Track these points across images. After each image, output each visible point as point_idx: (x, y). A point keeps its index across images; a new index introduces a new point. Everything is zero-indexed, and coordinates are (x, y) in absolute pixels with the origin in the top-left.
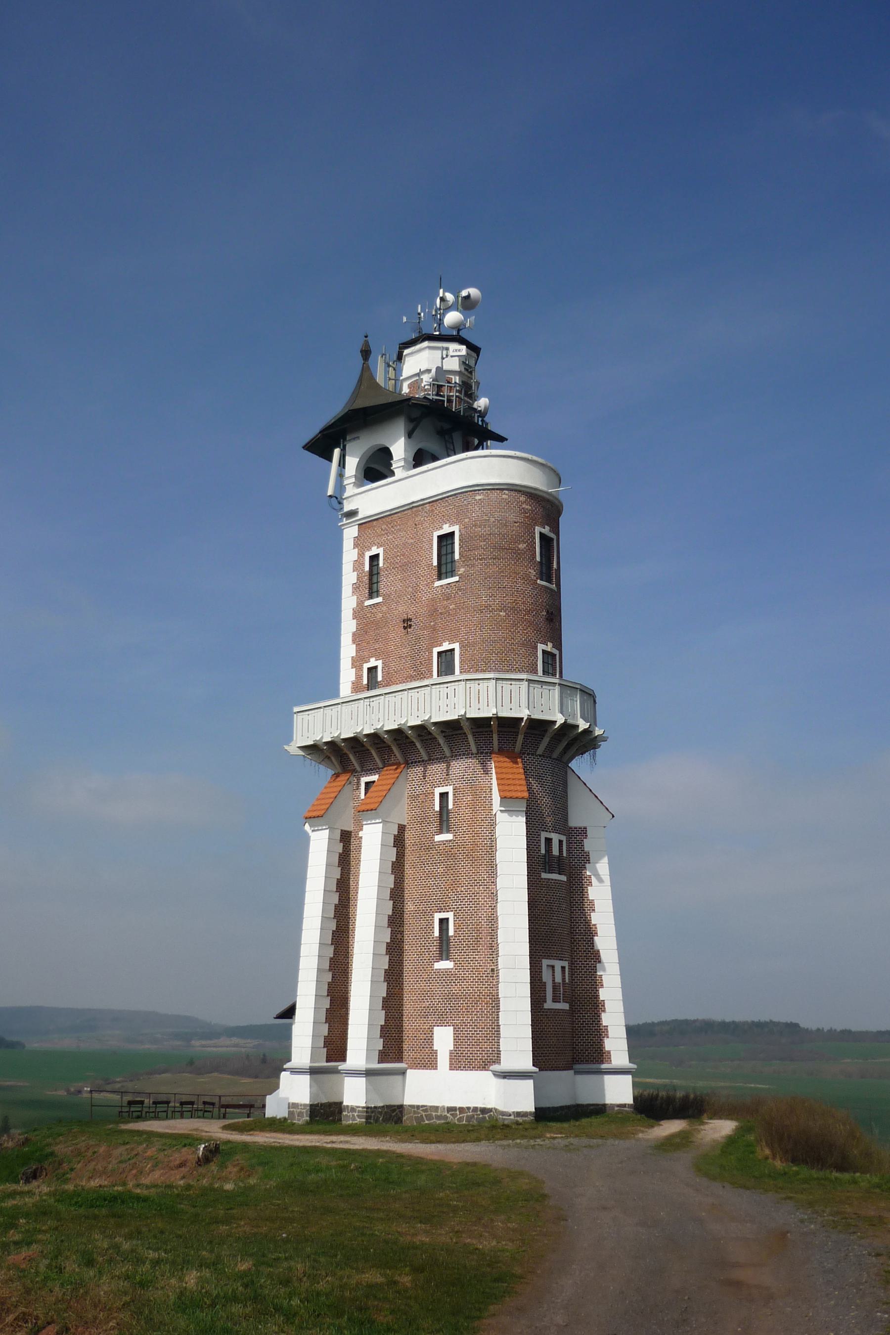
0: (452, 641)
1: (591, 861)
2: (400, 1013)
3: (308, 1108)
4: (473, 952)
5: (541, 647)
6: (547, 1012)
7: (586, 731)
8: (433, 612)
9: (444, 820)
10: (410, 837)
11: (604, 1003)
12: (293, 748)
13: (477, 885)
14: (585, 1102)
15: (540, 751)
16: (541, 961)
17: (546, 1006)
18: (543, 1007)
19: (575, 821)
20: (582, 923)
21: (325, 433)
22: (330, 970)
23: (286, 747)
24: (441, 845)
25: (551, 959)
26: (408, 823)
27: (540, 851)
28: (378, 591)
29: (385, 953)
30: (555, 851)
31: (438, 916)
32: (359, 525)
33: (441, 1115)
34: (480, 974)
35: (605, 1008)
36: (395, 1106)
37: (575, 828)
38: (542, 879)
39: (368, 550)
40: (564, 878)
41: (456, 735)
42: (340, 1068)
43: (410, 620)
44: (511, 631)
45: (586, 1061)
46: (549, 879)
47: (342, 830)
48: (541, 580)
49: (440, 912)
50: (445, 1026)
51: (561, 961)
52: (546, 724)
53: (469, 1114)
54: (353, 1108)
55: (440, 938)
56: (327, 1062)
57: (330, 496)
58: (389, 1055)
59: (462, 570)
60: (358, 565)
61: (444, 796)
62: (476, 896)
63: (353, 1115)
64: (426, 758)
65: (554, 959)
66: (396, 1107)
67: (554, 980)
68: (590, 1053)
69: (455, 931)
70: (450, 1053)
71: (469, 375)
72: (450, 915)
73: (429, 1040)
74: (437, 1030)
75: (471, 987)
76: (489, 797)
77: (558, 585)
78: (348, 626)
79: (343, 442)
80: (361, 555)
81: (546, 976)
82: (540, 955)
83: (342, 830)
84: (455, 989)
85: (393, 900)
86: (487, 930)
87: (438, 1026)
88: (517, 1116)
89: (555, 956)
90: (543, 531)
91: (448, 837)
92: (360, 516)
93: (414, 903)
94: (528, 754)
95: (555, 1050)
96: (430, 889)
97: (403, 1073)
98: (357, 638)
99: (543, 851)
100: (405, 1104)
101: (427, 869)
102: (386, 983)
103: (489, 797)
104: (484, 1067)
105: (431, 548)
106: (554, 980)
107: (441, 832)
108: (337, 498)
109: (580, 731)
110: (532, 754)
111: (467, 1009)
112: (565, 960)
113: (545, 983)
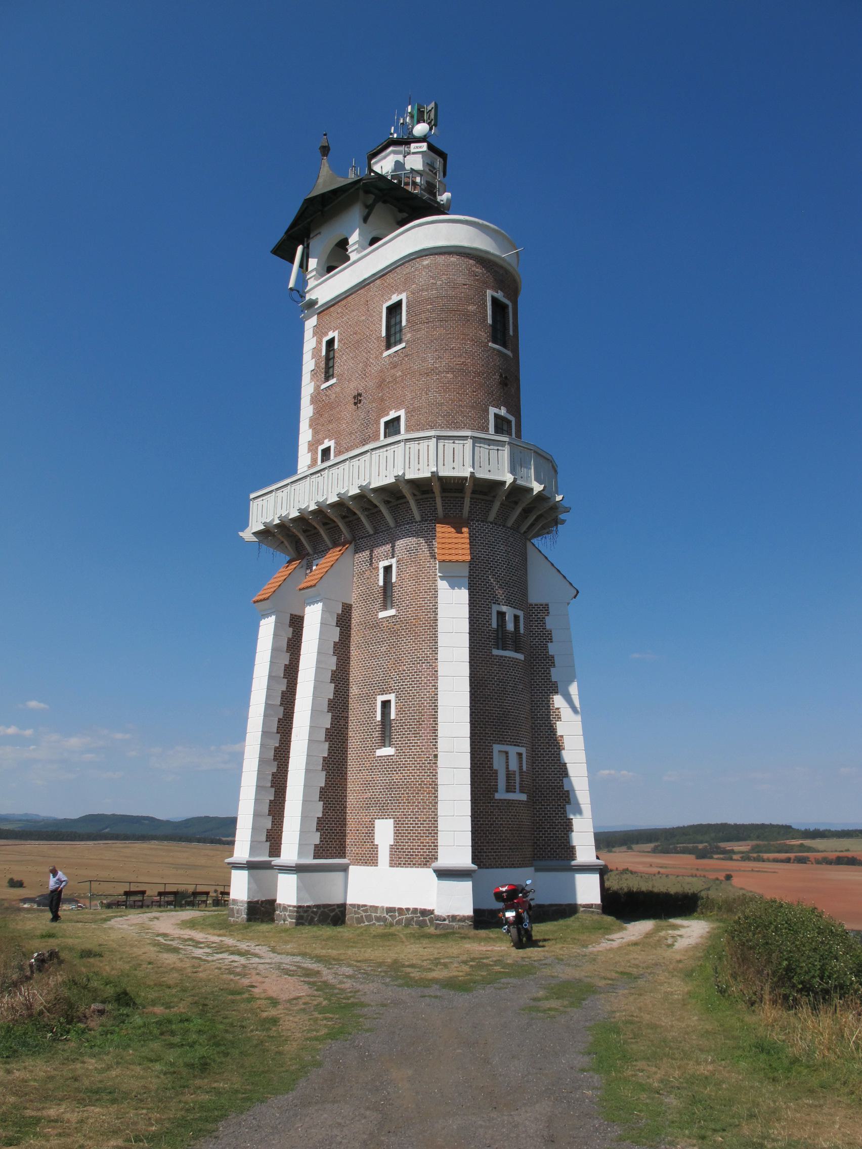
0: (398, 409)
1: (554, 640)
2: (343, 804)
3: (246, 905)
4: (415, 737)
5: (492, 410)
6: (498, 803)
7: (541, 496)
8: (381, 385)
9: (387, 594)
10: (356, 617)
11: (569, 794)
12: (247, 535)
13: (419, 663)
14: (546, 902)
15: (492, 516)
16: (492, 746)
17: (497, 796)
18: (494, 797)
19: (535, 597)
20: (544, 706)
21: (289, 233)
22: (275, 760)
23: (241, 534)
24: (384, 622)
25: (504, 744)
26: (354, 602)
27: (491, 625)
28: (333, 375)
29: (324, 739)
30: (510, 626)
31: (380, 698)
32: (319, 314)
33: (381, 916)
34: (422, 761)
35: (569, 800)
36: (334, 905)
37: (535, 605)
38: (493, 655)
39: (325, 336)
40: (521, 657)
41: (401, 504)
42: (273, 863)
43: (360, 395)
44: (459, 393)
45: (548, 857)
46: (502, 656)
47: (291, 615)
48: (495, 342)
49: (382, 694)
50: (386, 818)
51: (517, 747)
52: (496, 485)
53: (408, 916)
54: (285, 907)
55: (382, 722)
56: (315, 857)
57: (291, 289)
58: (328, 850)
59: (409, 335)
60: (316, 351)
61: (388, 569)
62: (419, 675)
63: (285, 915)
64: (371, 532)
65: (507, 744)
66: (335, 907)
67: (507, 768)
68: (553, 849)
69: (397, 715)
70: (391, 848)
71: (434, 175)
72: (392, 697)
73: (370, 833)
74: (378, 823)
75: (412, 776)
76: (433, 567)
77: (516, 351)
78: (307, 411)
79: (307, 241)
80: (319, 342)
81: (498, 763)
82: (491, 740)
83: (291, 615)
84: (396, 777)
85: (334, 683)
86: (429, 712)
87: (379, 818)
88: (452, 921)
89: (509, 741)
90: (495, 294)
91: (392, 612)
92: (320, 304)
93: (359, 686)
94: (477, 521)
95: (508, 846)
96: (373, 670)
97: (344, 869)
98: (313, 423)
99: (494, 625)
100: (349, 901)
101: (371, 649)
102: (325, 773)
103: (433, 567)
104: (425, 864)
105: (381, 321)
106: (507, 768)
107: (385, 608)
108: (298, 292)
109: (534, 494)
110: (482, 521)
111: (408, 800)
112: (522, 746)
113: (496, 771)
